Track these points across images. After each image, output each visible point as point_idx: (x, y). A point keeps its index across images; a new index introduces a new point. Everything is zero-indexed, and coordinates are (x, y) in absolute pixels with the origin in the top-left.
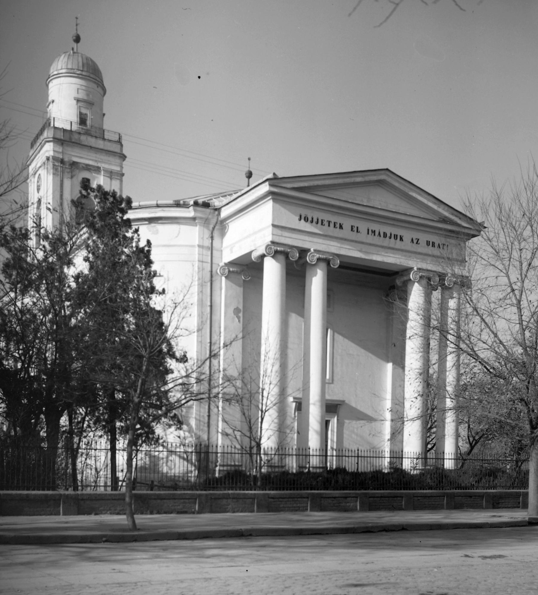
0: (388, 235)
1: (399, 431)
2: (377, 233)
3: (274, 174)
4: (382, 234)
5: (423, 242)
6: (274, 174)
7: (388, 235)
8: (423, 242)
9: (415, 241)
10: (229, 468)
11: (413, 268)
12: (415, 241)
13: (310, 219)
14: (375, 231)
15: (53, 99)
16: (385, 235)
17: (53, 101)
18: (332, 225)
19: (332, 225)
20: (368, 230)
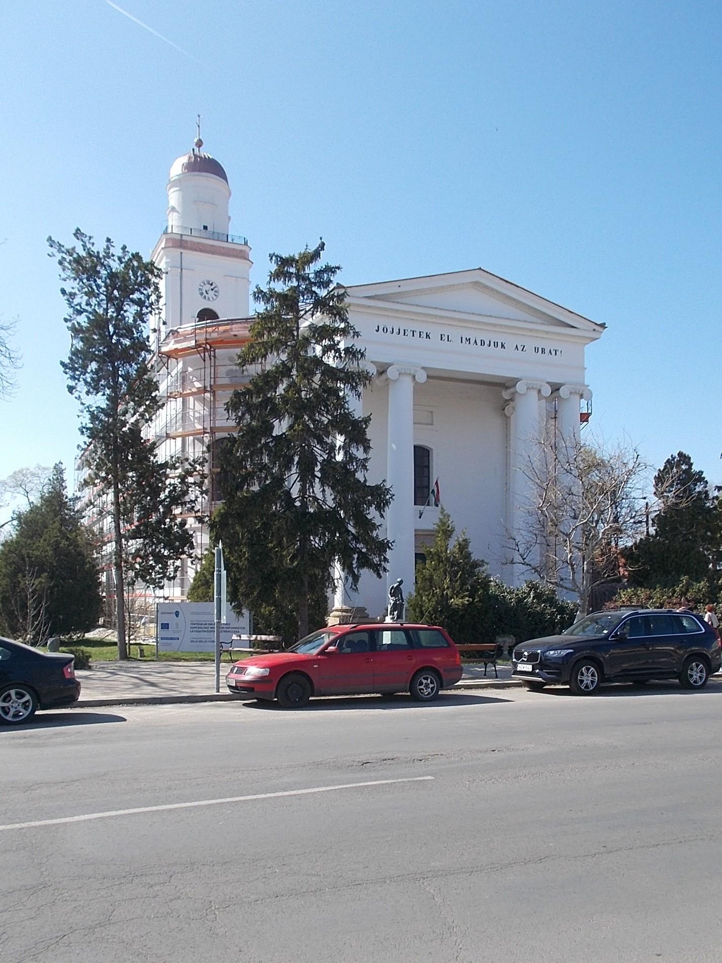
0: (487, 343)
1: (212, 358)
2: (472, 341)
3: (367, 420)
4: (479, 343)
5: (530, 349)
6: (367, 420)
7: (487, 343)
8: (530, 349)
9: (520, 348)
10: (162, 600)
11: (89, 474)
12: (520, 348)
13: (390, 330)
14: (469, 339)
15: (95, 242)
16: (483, 343)
17: (78, 233)
18: (417, 334)
19: (417, 334)
20: (462, 338)
